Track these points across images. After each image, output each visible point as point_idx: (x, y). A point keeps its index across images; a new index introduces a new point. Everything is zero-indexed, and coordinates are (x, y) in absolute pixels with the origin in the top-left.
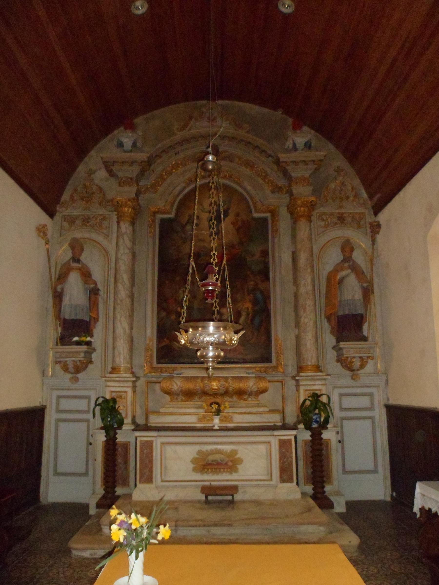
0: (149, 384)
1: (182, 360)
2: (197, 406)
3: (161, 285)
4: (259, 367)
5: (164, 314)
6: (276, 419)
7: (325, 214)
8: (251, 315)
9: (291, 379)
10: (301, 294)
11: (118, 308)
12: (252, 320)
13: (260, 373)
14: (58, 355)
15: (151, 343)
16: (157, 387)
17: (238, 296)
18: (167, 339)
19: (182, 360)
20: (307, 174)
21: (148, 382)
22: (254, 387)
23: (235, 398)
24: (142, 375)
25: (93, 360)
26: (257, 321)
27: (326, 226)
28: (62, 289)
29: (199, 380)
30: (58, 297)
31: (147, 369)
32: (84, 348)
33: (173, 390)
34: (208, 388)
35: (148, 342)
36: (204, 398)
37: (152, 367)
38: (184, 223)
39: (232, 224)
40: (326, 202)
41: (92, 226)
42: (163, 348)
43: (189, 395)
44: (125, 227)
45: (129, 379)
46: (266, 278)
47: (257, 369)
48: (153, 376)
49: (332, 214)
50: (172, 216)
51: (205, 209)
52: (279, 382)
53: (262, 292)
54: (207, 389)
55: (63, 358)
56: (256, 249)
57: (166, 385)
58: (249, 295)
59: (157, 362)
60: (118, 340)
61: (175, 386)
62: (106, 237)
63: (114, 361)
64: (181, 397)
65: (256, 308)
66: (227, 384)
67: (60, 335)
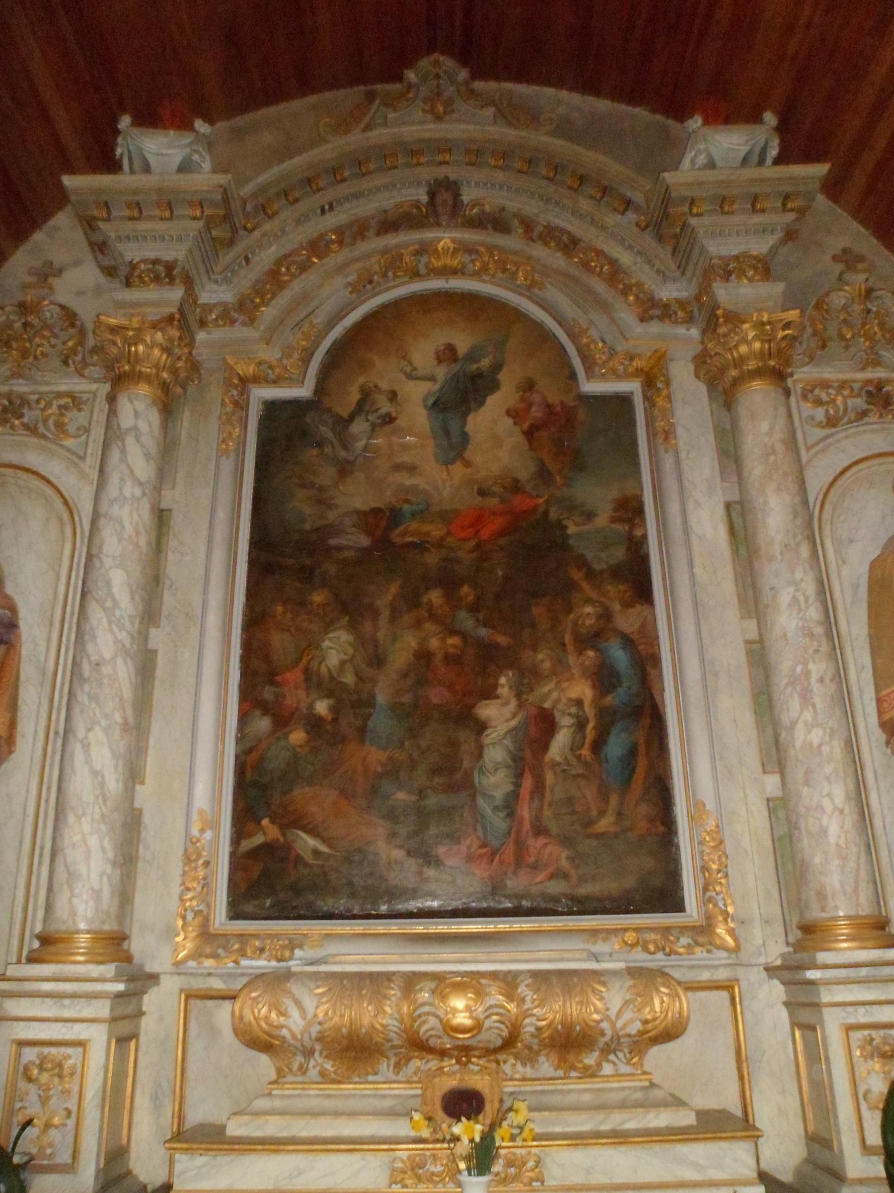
0: (195, 1004)
1: (327, 904)
2: (387, 1103)
3: (255, 620)
4: (637, 930)
5: (262, 724)
7: (825, 385)
8: (591, 725)
9: (764, 974)
10: (785, 636)
12: (598, 745)
13: (646, 956)
15: (208, 835)
16: (223, 1013)
17: (540, 656)
18: (273, 822)
19: (327, 904)
20: (760, 246)
21: (191, 996)
22: (627, 1015)
23: (546, 1066)
24: (168, 967)
26: (615, 747)
27: (832, 422)
29: (395, 992)
31: (185, 943)
33: (285, 1032)
34: (432, 1021)
35: (195, 832)
36: (416, 1063)
37: (206, 935)
38: (345, 414)
39: (508, 413)
40: (824, 346)
41: (32, 429)
42: (253, 854)
43: (355, 1052)
44: (138, 410)
45: (98, 987)
46: (643, 592)
47: (630, 937)
48: (215, 973)
49: (843, 384)
50: (304, 392)
51: (415, 369)
52: (718, 988)
53: (628, 642)
54: (429, 1027)
56: (597, 495)
57: (259, 1011)
58: (580, 653)
59: (229, 911)
61: (295, 1013)
62: (76, 460)
64: (319, 1062)
65: (609, 700)
66: (512, 1007)
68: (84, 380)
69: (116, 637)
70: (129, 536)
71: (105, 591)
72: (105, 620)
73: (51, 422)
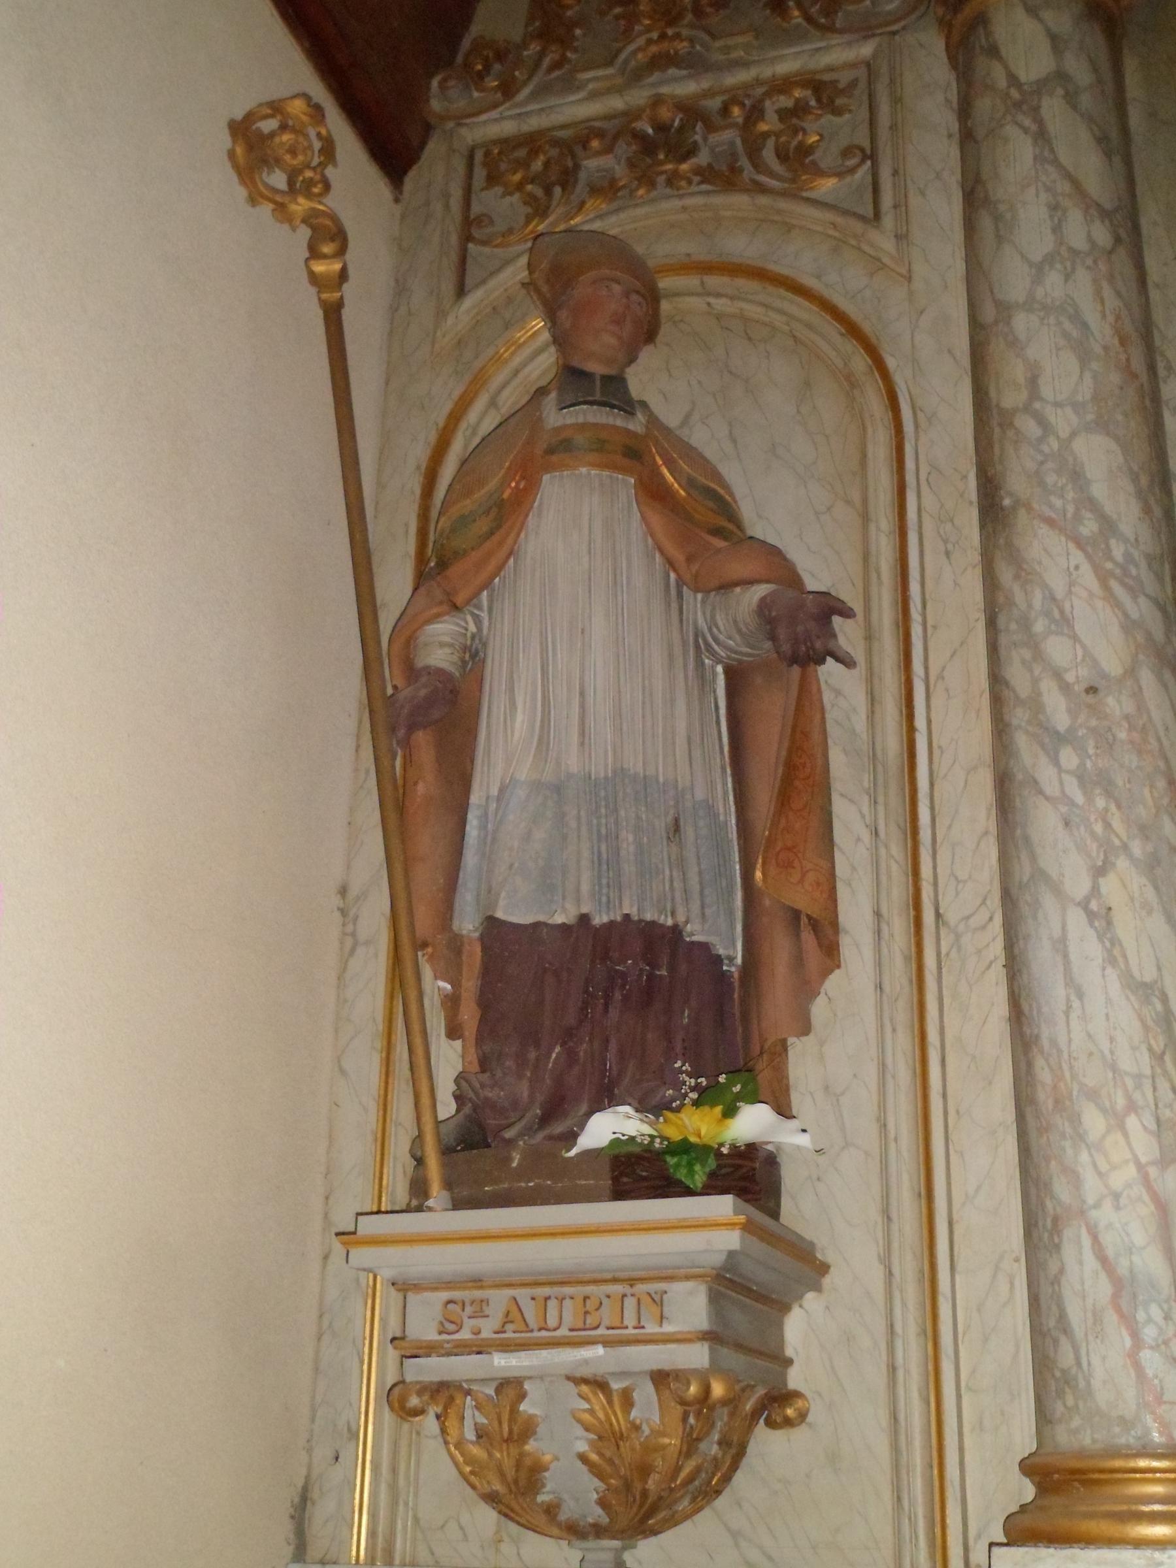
6: (319, 1399)
11: (1052, 776)
14: (424, 1323)
25: (795, 1379)
28: (473, 656)
30: (424, 725)
32: (707, 1226)
55: (481, 1348)
60: (1094, 1122)
63: (1051, 1379)
67: (447, 1108)
68: (836, 39)
69: (1126, 615)
70: (1106, 348)
71: (1070, 495)
72: (1086, 569)
73: (768, 154)
